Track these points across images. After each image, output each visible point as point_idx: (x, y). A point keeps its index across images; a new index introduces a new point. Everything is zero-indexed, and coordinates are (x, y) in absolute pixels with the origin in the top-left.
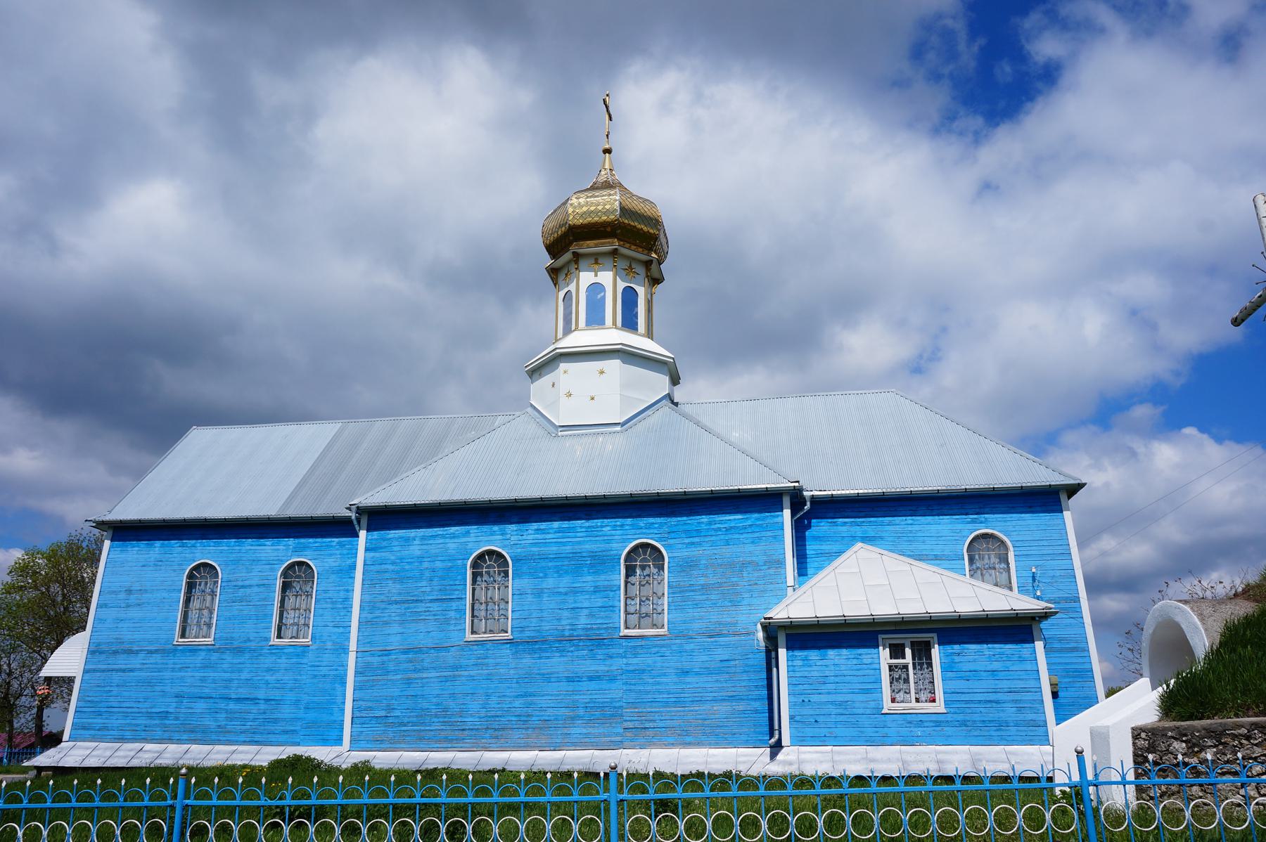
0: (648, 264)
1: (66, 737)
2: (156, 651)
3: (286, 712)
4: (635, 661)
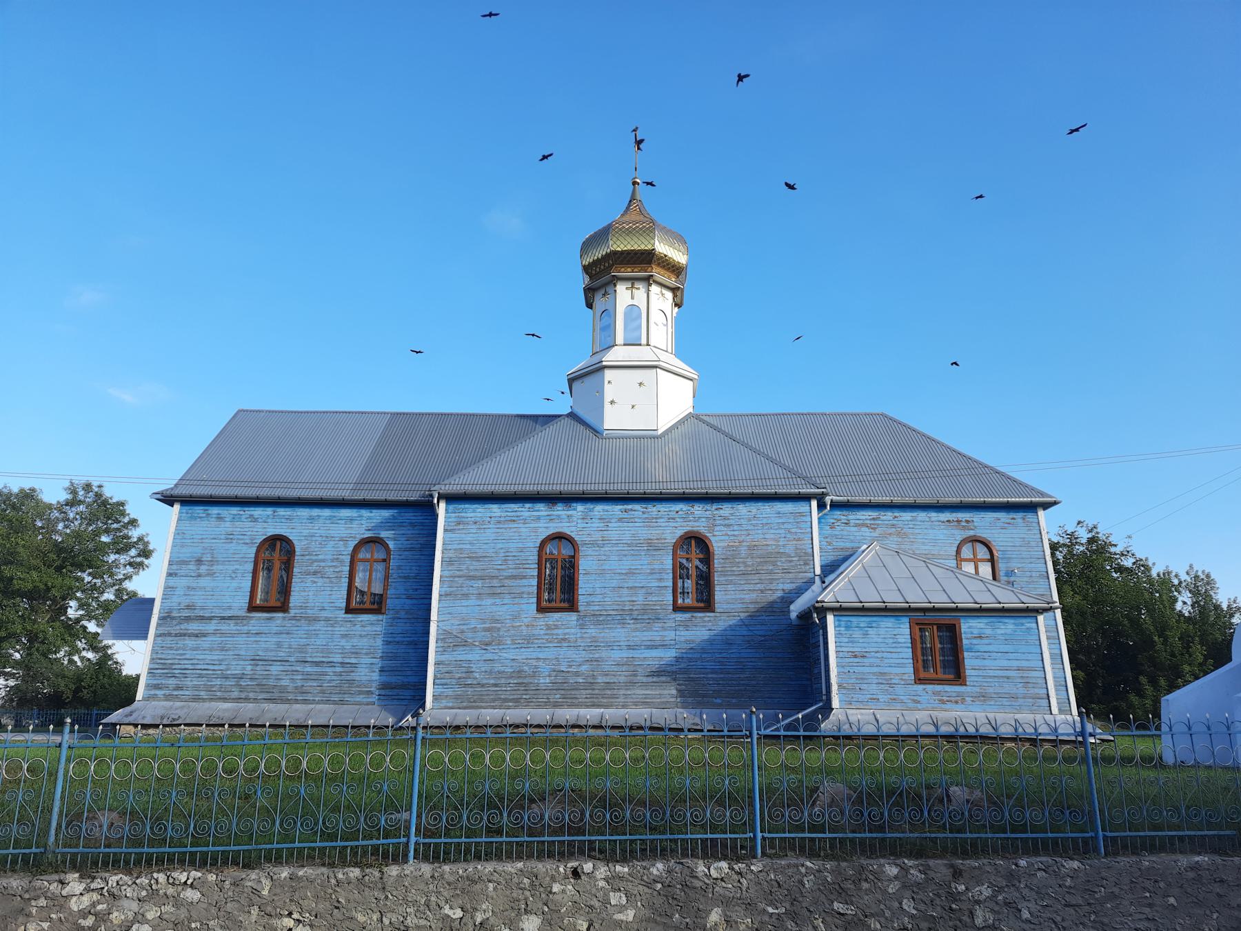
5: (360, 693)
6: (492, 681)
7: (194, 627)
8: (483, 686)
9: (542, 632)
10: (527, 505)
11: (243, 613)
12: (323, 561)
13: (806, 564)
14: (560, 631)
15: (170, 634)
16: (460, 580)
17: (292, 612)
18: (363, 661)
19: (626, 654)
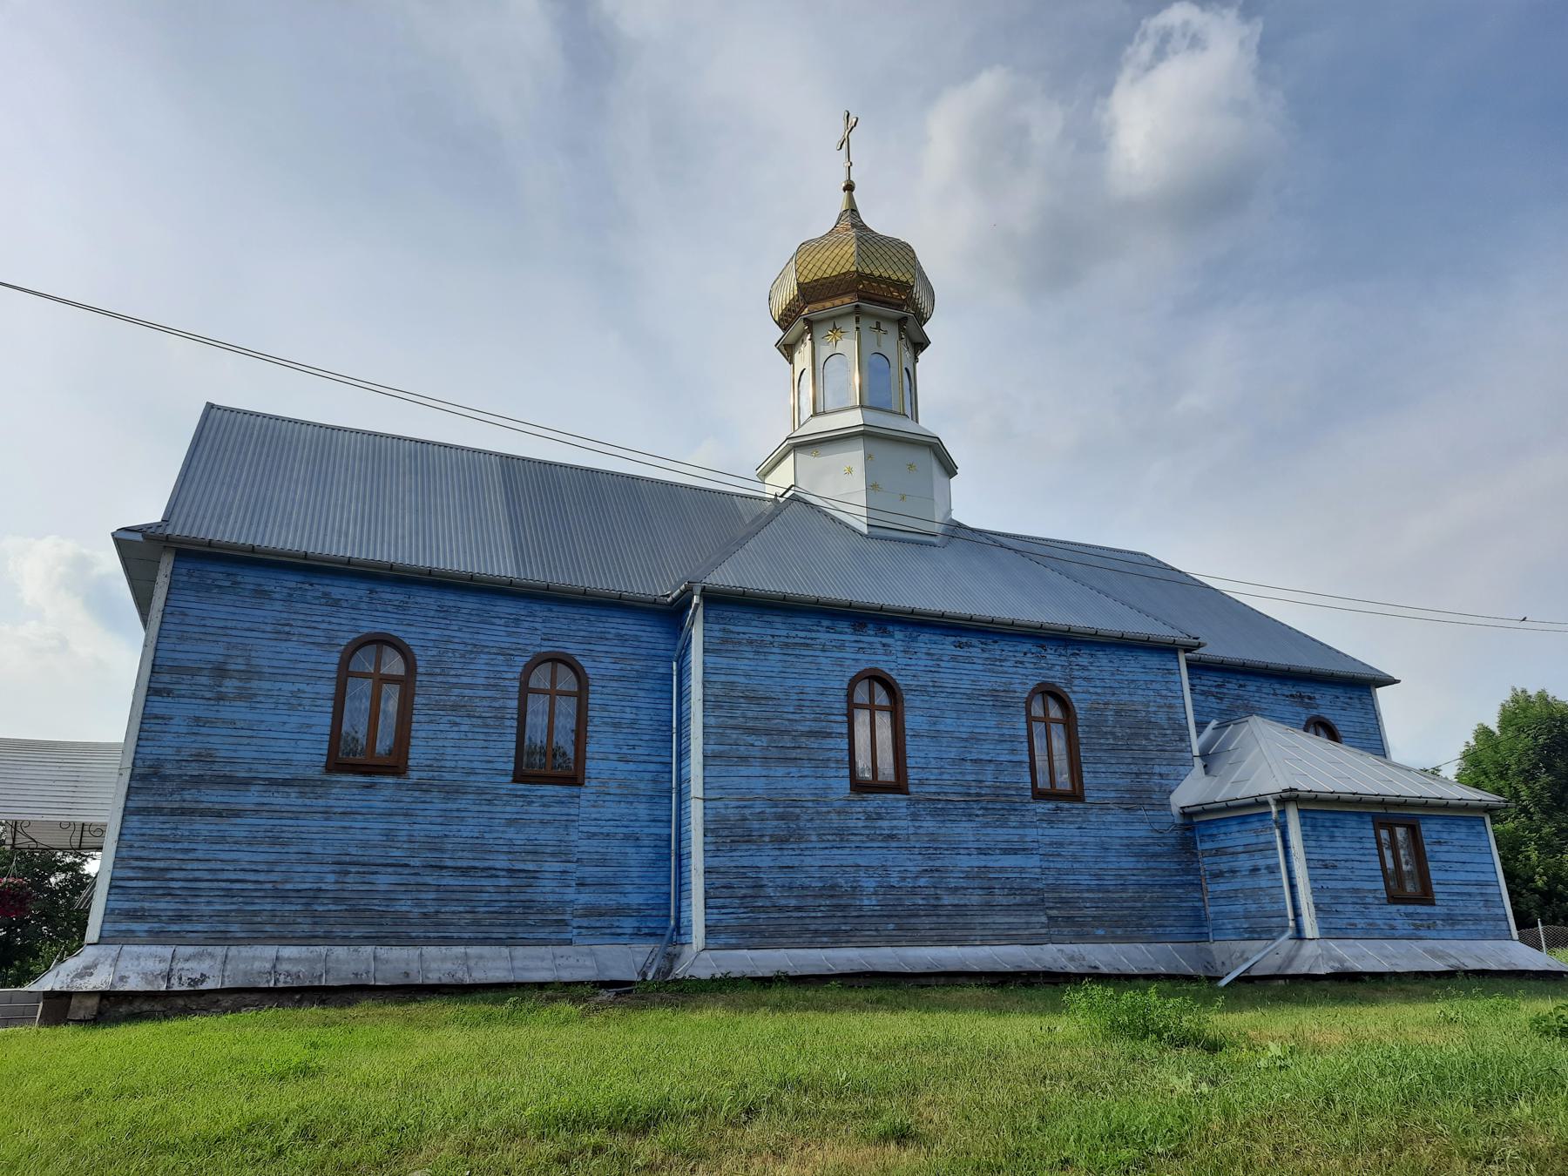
0: (901, 322)
1: (92, 933)
2: (286, 783)
3: (546, 891)
4: (1052, 832)
5: (545, 923)
6: (793, 902)
7: (214, 797)
8: (781, 909)
9: (860, 824)
10: (826, 623)
11: (315, 773)
12: (470, 686)
13: (1182, 740)
14: (885, 824)
15: (159, 811)
16: (734, 734)
17: (414, 776)
18: (546, 866)
19: (977, 861)
